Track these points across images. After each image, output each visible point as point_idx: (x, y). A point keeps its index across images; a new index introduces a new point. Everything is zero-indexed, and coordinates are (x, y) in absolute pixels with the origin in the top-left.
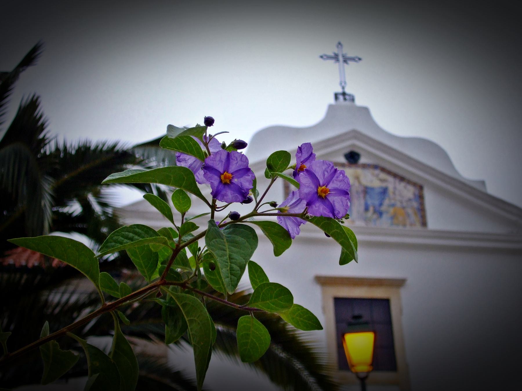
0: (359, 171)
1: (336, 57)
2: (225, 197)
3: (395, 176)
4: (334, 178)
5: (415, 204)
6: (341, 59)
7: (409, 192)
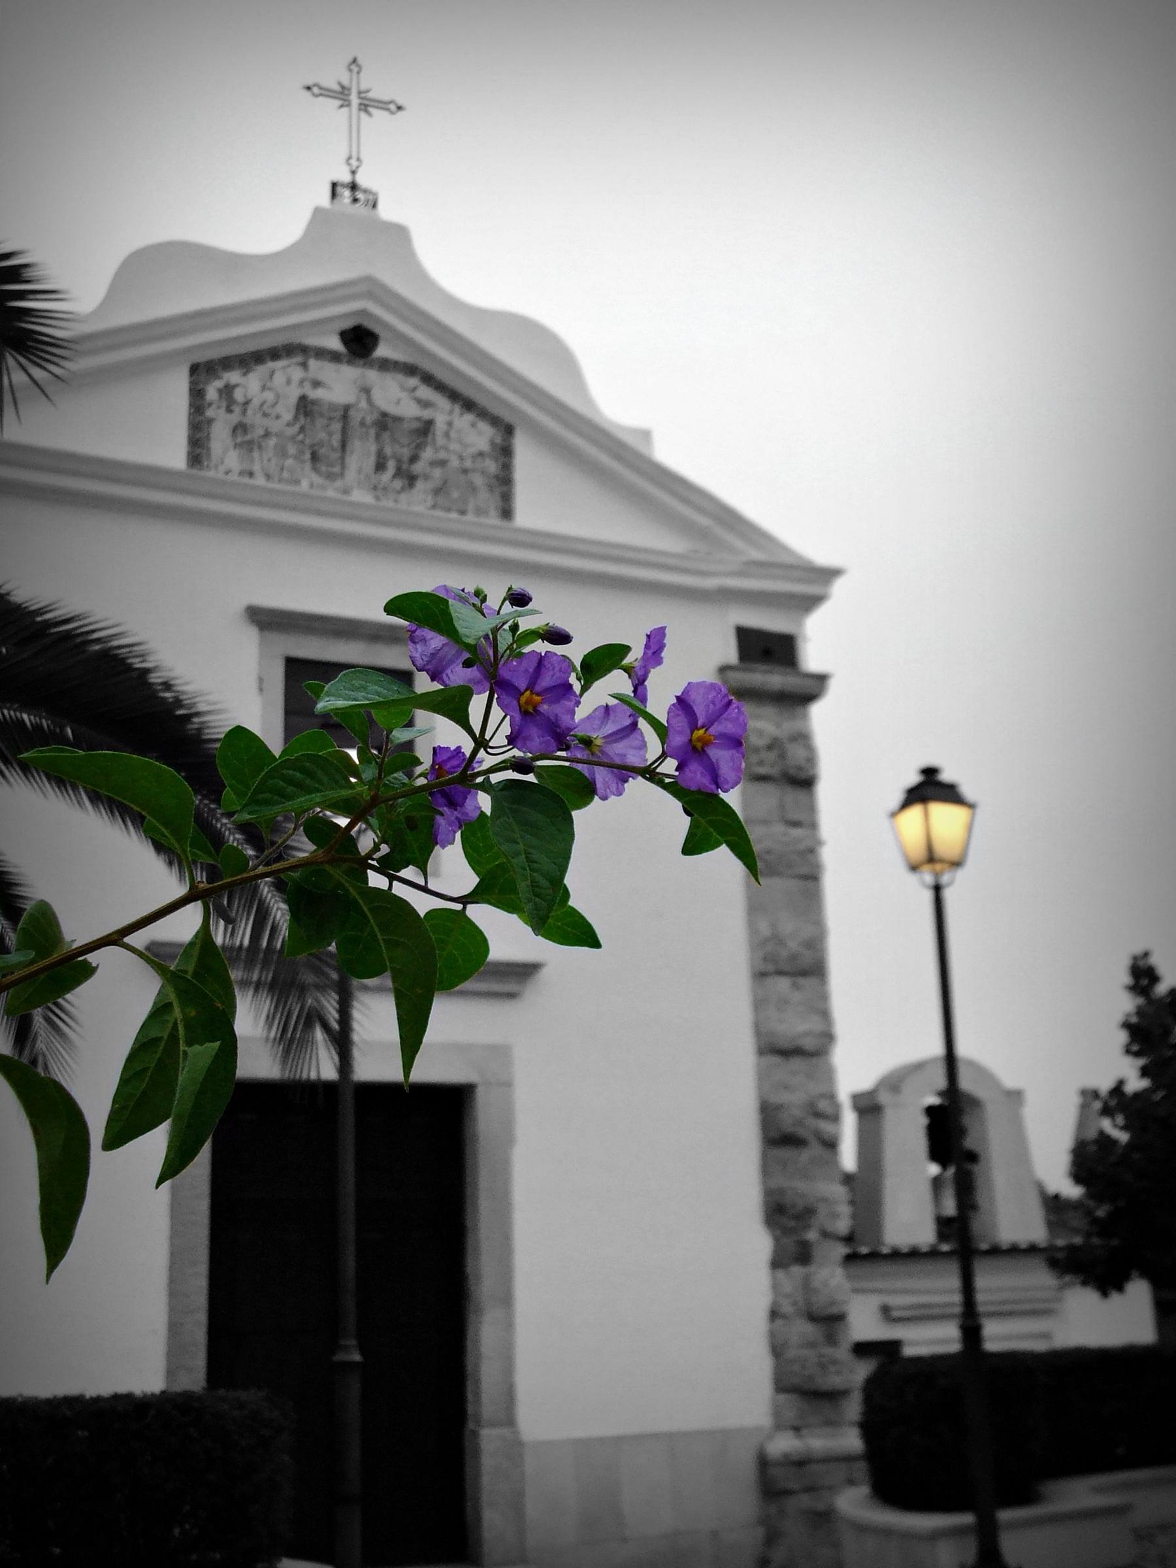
1: (342, 94)
2: (528, 743)
3: (454, 396)
5: (492, 467)
6: (355, 100)
7: (481, 437)
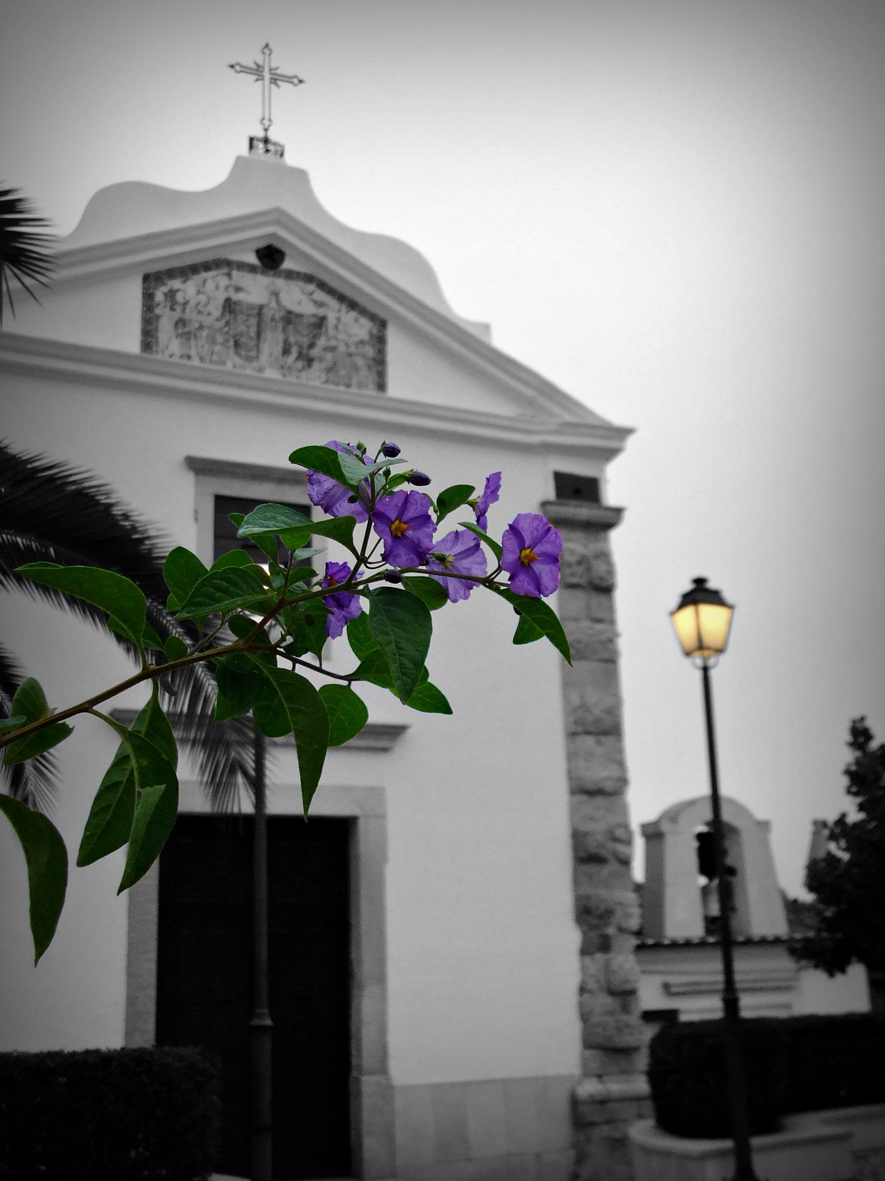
0: (280, 283)
1: (257, 71)
2: (398, 560)
3: (342, 298)
4: (545, 539)
5: (370, 351)
6: (267, 76)
7: (362, 329)
